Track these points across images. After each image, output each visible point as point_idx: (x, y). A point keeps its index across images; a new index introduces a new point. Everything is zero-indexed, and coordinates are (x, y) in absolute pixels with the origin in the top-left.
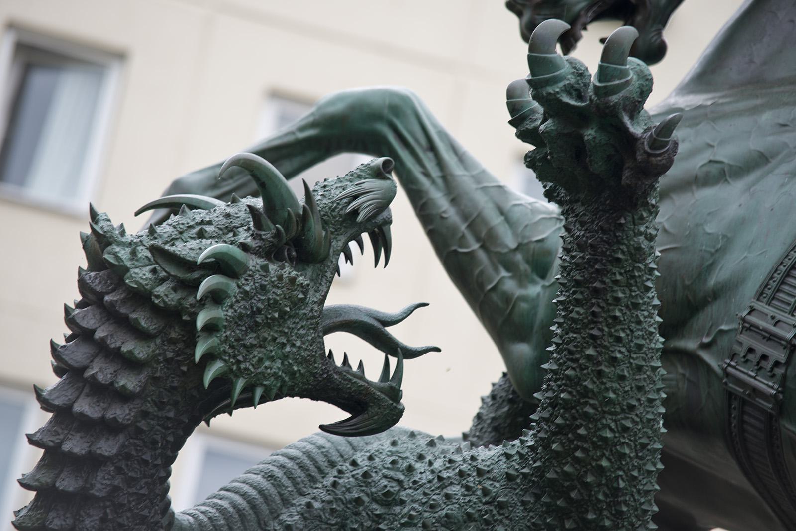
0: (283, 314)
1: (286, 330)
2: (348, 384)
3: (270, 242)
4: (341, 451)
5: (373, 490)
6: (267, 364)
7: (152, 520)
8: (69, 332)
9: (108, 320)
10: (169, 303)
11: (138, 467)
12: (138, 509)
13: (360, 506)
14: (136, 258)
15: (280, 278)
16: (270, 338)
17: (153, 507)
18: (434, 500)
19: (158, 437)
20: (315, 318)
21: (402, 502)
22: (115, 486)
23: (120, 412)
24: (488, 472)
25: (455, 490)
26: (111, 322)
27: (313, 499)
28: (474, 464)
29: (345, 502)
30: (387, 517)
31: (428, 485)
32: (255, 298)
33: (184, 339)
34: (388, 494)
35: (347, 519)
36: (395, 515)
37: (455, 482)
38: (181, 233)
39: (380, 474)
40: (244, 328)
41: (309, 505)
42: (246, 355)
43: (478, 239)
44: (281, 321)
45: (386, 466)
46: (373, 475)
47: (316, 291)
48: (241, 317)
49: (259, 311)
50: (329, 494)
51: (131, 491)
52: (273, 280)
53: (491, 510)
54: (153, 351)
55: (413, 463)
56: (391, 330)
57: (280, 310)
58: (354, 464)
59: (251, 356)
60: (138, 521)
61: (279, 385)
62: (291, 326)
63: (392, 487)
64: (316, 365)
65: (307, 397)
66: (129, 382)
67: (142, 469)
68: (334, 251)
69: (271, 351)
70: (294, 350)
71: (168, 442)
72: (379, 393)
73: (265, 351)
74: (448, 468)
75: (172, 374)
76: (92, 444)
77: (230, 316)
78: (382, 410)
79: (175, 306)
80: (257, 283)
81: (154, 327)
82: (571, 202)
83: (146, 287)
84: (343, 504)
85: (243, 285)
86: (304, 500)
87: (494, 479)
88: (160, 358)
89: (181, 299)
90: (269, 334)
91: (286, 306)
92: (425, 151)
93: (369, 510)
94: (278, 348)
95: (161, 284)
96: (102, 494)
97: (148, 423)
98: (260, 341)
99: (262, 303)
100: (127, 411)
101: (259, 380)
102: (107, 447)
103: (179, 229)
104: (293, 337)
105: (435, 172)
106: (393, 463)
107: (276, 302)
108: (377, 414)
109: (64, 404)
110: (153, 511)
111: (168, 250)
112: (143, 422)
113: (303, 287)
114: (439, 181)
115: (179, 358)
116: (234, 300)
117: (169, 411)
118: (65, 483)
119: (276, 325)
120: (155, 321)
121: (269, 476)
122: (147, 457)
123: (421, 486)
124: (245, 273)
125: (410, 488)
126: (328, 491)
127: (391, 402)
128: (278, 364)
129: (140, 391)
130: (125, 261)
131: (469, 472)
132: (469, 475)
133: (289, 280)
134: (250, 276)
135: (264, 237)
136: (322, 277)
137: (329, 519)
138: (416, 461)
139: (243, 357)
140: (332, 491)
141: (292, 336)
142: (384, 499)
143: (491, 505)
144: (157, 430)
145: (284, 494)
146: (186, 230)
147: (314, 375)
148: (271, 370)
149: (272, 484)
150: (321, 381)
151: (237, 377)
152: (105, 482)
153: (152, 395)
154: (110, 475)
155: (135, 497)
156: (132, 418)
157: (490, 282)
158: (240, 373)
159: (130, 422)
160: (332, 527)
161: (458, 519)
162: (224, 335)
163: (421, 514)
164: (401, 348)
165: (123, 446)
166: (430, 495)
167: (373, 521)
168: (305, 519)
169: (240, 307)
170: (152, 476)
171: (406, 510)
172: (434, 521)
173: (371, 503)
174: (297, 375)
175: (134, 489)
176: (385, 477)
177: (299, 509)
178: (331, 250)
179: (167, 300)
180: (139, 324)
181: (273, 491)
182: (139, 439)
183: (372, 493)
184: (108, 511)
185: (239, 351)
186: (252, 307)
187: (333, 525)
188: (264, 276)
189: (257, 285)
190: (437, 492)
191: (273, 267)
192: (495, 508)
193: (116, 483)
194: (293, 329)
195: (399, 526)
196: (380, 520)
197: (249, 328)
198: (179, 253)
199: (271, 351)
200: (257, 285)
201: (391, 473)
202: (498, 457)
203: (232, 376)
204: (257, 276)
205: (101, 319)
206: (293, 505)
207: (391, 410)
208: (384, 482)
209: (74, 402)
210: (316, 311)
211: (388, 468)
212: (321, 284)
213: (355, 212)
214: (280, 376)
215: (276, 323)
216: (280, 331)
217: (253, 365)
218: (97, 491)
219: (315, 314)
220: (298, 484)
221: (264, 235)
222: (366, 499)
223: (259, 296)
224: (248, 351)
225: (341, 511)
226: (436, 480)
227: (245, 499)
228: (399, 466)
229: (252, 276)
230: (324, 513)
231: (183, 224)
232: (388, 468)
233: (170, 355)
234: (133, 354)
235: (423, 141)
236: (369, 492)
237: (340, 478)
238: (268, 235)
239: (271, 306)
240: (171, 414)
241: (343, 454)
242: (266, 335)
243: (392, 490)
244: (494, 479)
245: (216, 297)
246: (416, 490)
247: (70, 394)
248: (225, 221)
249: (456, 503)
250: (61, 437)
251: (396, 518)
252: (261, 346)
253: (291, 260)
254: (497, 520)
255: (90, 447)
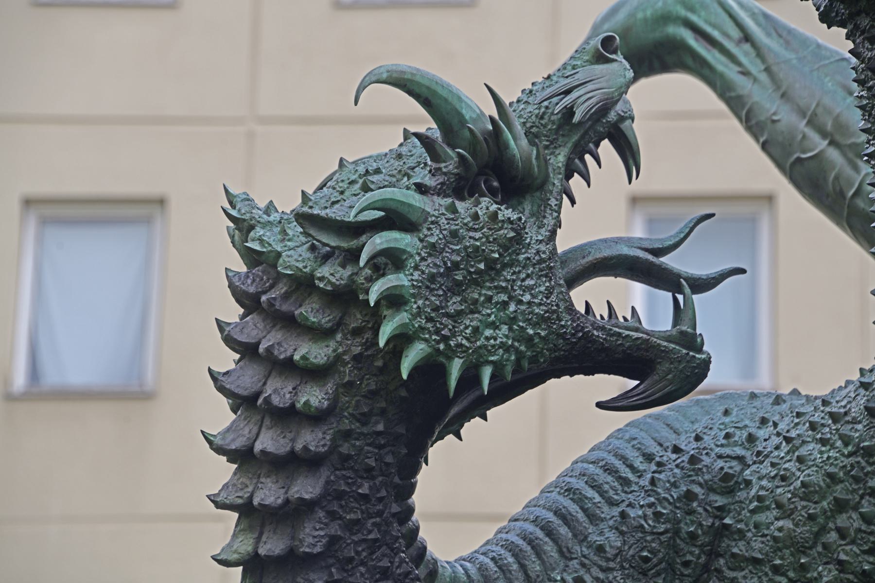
0: (491, 264)
1: (504, 284)
2: (617, 340)
3: (456, 175)
4: (658, 439)
5: (707, 477)
6: (488, 332)
7: (398, 571)
8: (238, 356)
9: (274, 326)
10: (338, 283)
11: (357, 505)
12: (373, 560)
13: (693, 501)
14: (287, 238)
15: (476, 217)
16: (482, 299)
17: (396, 554)
18: (785, 469)
19: (372, 462)
20: (545, 262)
21: (748, 483)
22: (333, 536)
23: (311, 439)
24: (846, 414)
25: (811, 449)
26: (278, 327)
27: (628, 506)
28: (828, 409)
29: (671, 501)
30: (732, 507)
31: (776, 453)
32: (447, 249)
33: (370, 326)
34: (727, 477)
35: (679, 522)
36: (741, 502)
37: (809, 439)
38: (342, 193)
39: (713, 455)
40: (441, 292)
41: (623, 515)
42: (454, 327)
43: (824, 134)
44: (493, 273)
45: (719, 443)
46: (704, 457)
47: (539, 228)
48: (432, 278)
49: (456, 266)
50: (649, 496)
51: (355, 538)
52: (465, 221)
53: (858, 462)
54: (334, 351)
55: (753, 430)
56: (666, 260)
57: (486, 258)
58: (677, 450)
59: (462, 328)
60: (377, 576)
61: (513, 358)
62: (509, 277)
63: (731, 468)
64: (563, 323)
65: (579, 374)
66: (314, 396)
67: (363, 507)
68: (554, 170)
69: (489, 315)
70: (523, 307)
71: (387, 464)
72: (665, 344)
73: (480, 317)
74: (797, 424)
75: (366, 375)
76: (288, 488)
77: (416, 281)
78: (676, 364)
79: (346, 285)
80: (445, 229)
81: (327, 319)
82: (852, 16)
83: (305, 270)
84: (670, 503)
85: (426, 236)
86: (616, 511)
87: (855, 421)
88: (345, 357)
89: (352, 274)
90: (480, 294)
91: (493, 252)
92: (739, 42)
93: (706, 504)
94: (499, 310)
95: (324, 263)
96: (318, 549)
97: (354, 446)
98: (469, 305)
99: (458, 255)
100: (320, 435)
101: (481, 357)
102: (306, 488)
103: (338, 189)
104: (518, 292)
105: (755, 67)
106: (727, 436)
107: (477, 249)
108: (670, 371)
109: (244, 446)
110: (397, 560)
111: (318, 215)
112: (346, 445)
113: (511, 223)
114: (763, 77)
115: (369, 353)
116: (418, 258)
117: (377, 423)
118: (268, 546)
119: (487, 281)
120: (328, 311)
121: (566, 490)
122: (364, 490)
123: (767, 456)
124: (426, 220)
125: (755, 463)
126: (646, 491)
127: (684, 351)
128: (505, 328)
129: (329, 405)
130: (273, 243)
131: (823, 421)
132: (823, 425)
133: (488, 217)
134: (432, 223)
135: (444, 170)
136: (545, 207)
137: (654, 527)
138: (759, 427)
139: (450, 330)
140: (652, 490)
141: (515, 290)
142: (723, 485)
143: (857, 456)
144: (369, 452)
145: (588, 509)
146: (348, 188)
147: (562, 336)
148: (495, 339)
149: (571, 499)
150: (576, 343)
151: (450, 359)
152: (317, 533)
153: (348, 408)
154: (322, 523)
155: (364, 546)
156: (328, 443)
157: (852, 185)
158: (450, 354)
159: (326, 449)
160: (661, 538)
161: (819, 486)
162: (415, 306)
163: (772, 492)
164: (685, 279)
165: (328, 482)
166: (779, 464)
167: (716, 517)
168: (622, 533)
169: (428, 265)
170: (380, 514)
171: (753, 492)
172: (790, 496)
173: (708, 495)
174: (537, 340)
175: (359, 535)
176: (720, 457)
177: (611, 523)
178: (550, 170)
179: (334, 280)
180: (307, 319)
181: (573, 508)
182: (349, 469)
183: (706, 482)
184: (333, 570)
185: (441, 324)
186: (445, 263)
187: (662, 534)
188: (453, 219)
189: (445, 232)
190: (788, 458)
191: (460, 206)
192: (863, 458)
193: (333, 532)
194: (514, 281)
195: (748, 515)
196: (724, 514)
197: (449, 290)
198: (333, 216)
199: (489, 315)
200: (445, 232)
201: (727, 451)
202: (855, 391)
203: (442, 359)
204: (443, 221)
205: (265, 327)
206: (602, 520)
207: (688, 362)
208: (720, 463)
209: (255, 441)
210: (544, 252)
211: (722, 446)
212: (544, 217)
213: (569, 112)
214: (512, 346)
215: (487, 278)
216: (496, 287)
217: (467, 339)
218: (308, 546)
219: (543, 256)
220: (606, 492)
221: (445, 167)
222: (697, 489)
223: (451, 246)
224: (455, 322)
225: (668, 514)
226: (784, 443)
227: (537, 526)
228: (736, 438)
229: (437, 223)
230: (646, 521)
231: (343, 181)
232: (722, 446)
233: (357, 350)
234: (307, 359)
235: (735, 33)
236: (702, 481)
237: (660, 472)
238: (451, 167)
239: (472, 255)
240: (380, 427)
241: (661, 442)
242: (476, 296)
243: (731, 471)
244: (855, 421)
245: (392, 260)
246: (762, 462)
247: (247, 431)
248: (397, 163)
249: (813, 465)
250: (250, 489)
251: (744, 505)
252: (472, 312)
253: (493, 193)
254: (868, 472)
255: (286, 493)
